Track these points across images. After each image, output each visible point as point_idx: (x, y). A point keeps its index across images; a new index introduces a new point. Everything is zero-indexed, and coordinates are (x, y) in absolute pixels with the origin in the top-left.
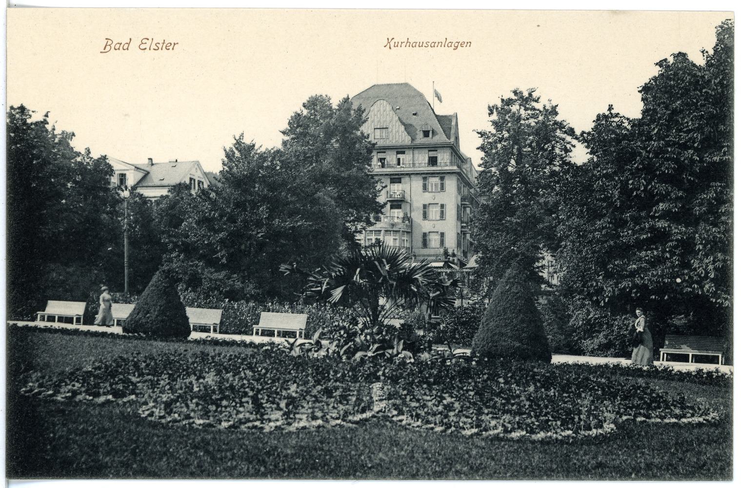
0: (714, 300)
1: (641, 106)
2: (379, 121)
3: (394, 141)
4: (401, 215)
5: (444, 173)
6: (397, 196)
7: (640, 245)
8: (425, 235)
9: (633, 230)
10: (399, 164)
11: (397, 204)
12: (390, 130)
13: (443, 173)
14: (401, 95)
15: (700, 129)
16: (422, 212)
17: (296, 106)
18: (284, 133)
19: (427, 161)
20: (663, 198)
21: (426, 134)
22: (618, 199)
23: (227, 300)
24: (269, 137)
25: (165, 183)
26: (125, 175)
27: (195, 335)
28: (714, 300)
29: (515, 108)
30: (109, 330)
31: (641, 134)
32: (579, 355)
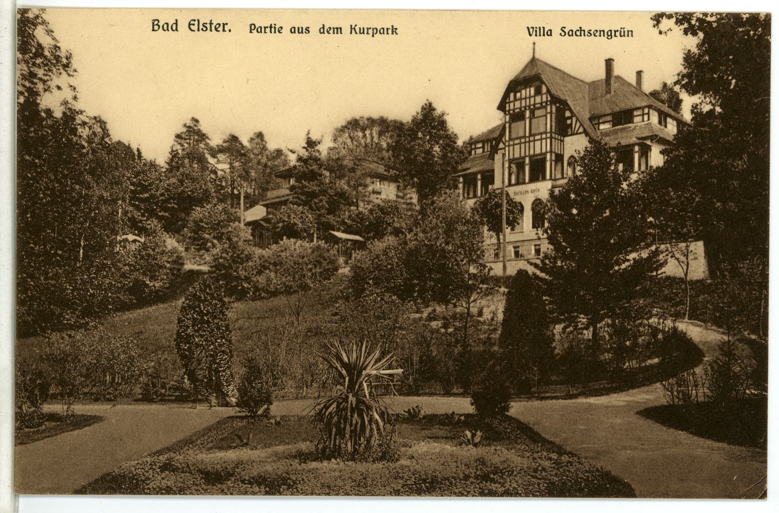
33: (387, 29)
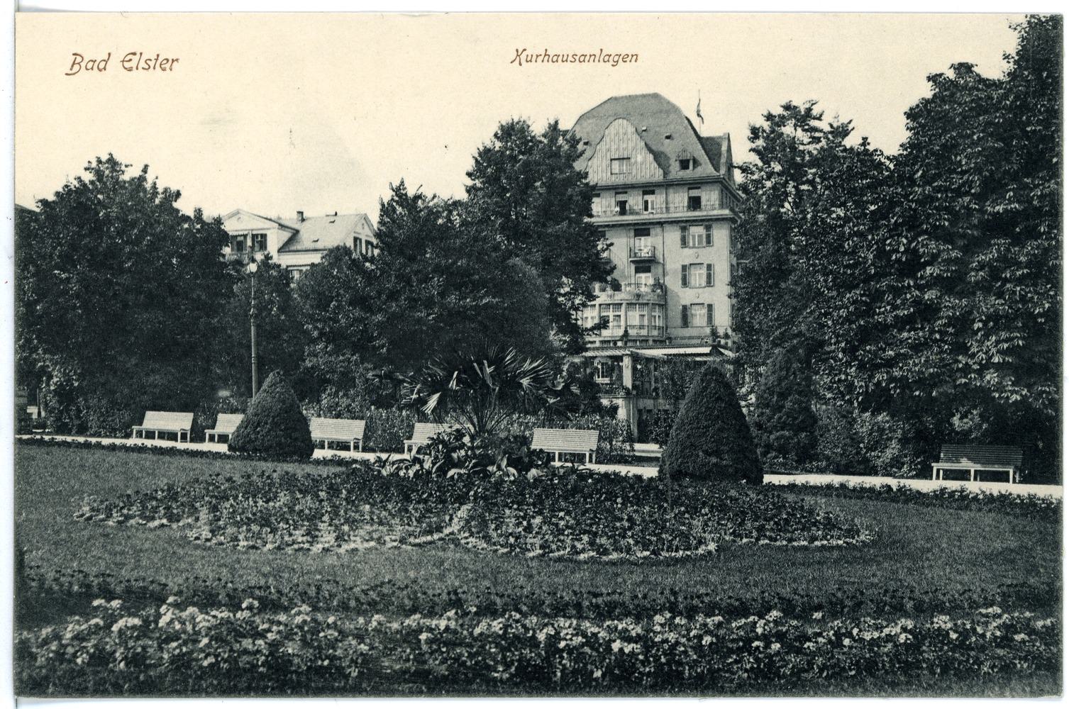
0: (997, 395)
1: (905, 136)
2: (618, 149)
4: (651, 282)
5: (711, 220)
6: (645, 254)
7: (902, 323)
8: (685, 308)
9: (892, 304)
10: (646, 209)
11: (643, 265)
12: (633, 160)
13: (708, 220)
14: (648, 111)
15: (978, 170)
16: (680, 276)
17: (485, 136)
18: (469, 174)
19: (686, 204)
20: (933, 260)
21: (684, 165)
22: (871, 264)
24: (446, 180)
25: (319, 245)
26: (266, 235)
27: (318, 454)
28: (997, 395)
29: (788, 130)
30: (206, 446)
31: (901, 178)
32: (870, 474)
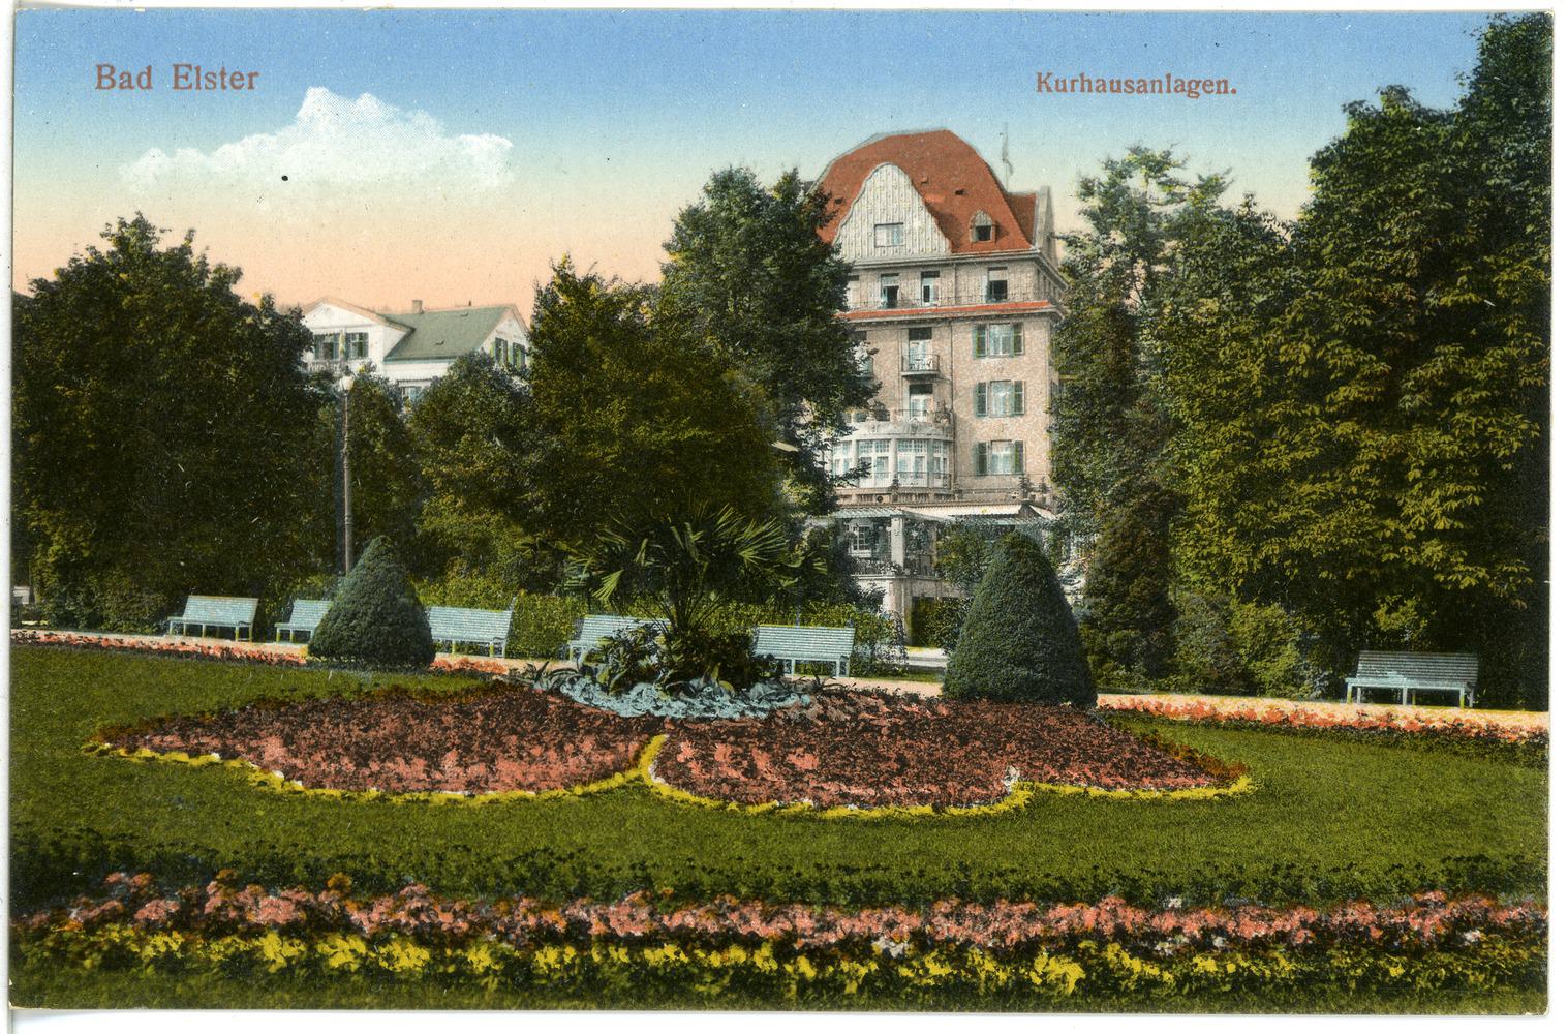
3: (915, 251)
4: (933, 407)
8: (982, 448)
19: (984, 293)
20: (1349, 375)
23: (522, 592)
25: (447, 349)
33: (1073, 81)
